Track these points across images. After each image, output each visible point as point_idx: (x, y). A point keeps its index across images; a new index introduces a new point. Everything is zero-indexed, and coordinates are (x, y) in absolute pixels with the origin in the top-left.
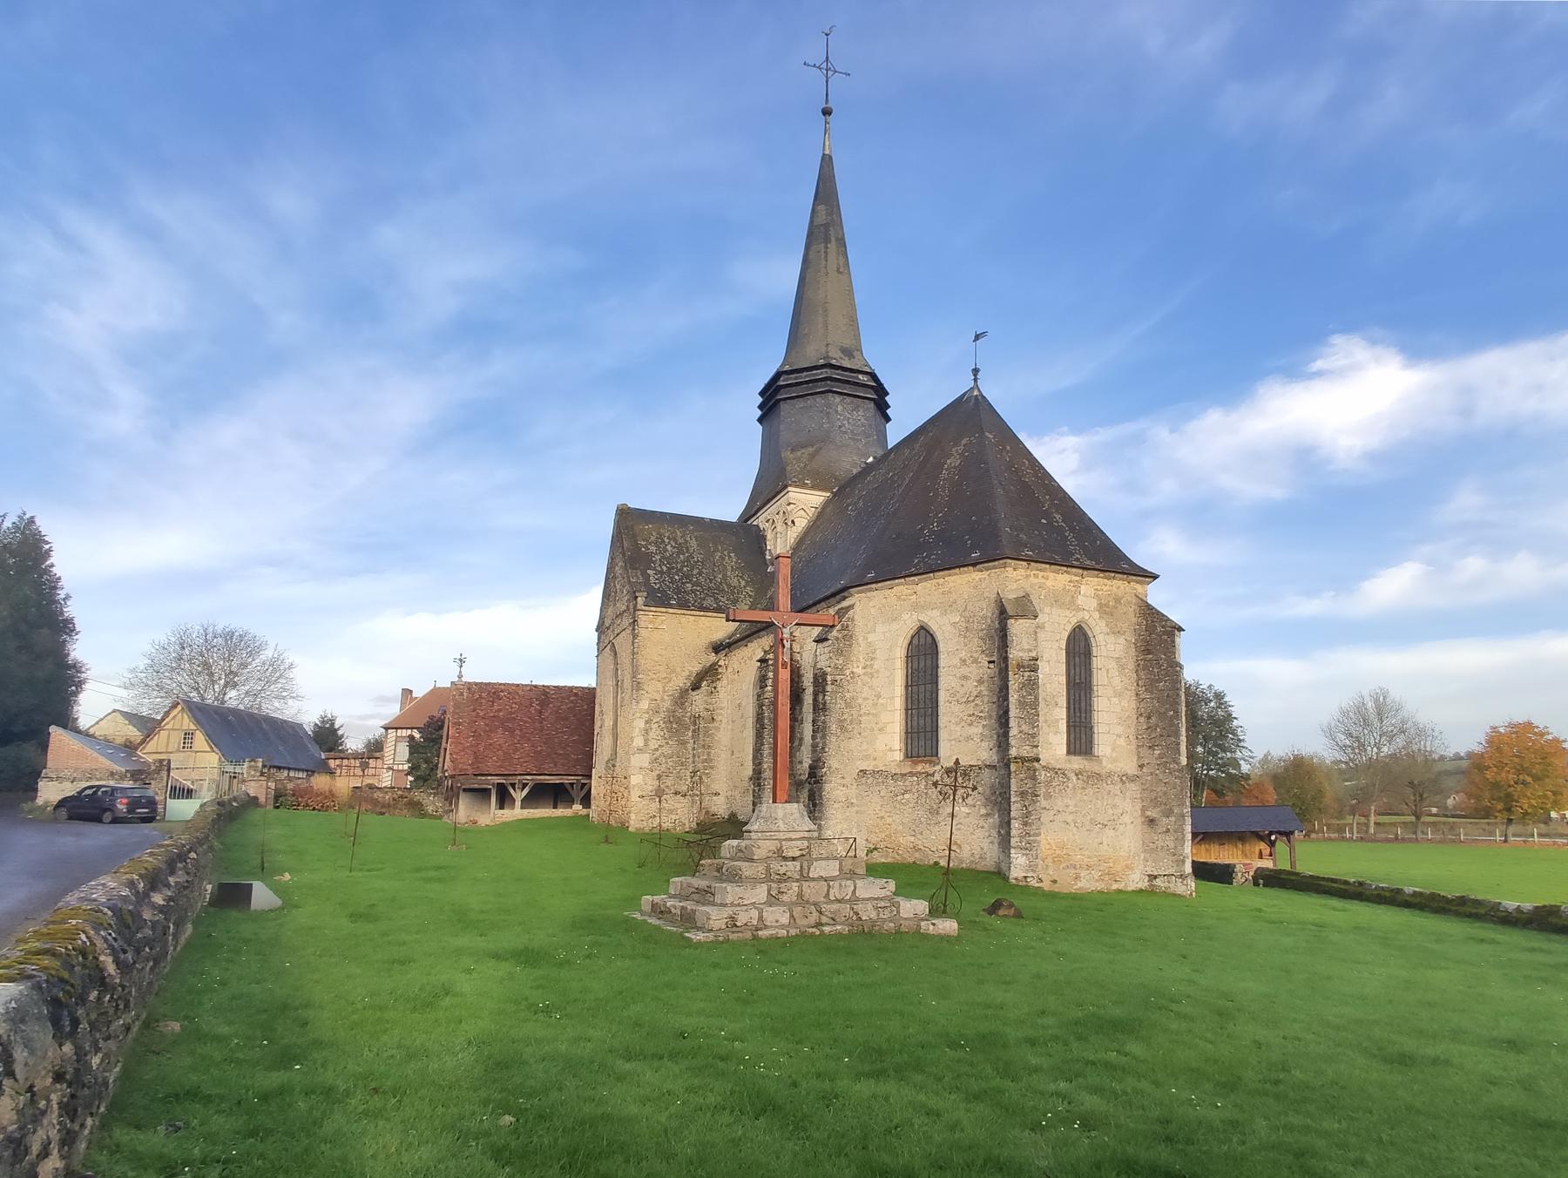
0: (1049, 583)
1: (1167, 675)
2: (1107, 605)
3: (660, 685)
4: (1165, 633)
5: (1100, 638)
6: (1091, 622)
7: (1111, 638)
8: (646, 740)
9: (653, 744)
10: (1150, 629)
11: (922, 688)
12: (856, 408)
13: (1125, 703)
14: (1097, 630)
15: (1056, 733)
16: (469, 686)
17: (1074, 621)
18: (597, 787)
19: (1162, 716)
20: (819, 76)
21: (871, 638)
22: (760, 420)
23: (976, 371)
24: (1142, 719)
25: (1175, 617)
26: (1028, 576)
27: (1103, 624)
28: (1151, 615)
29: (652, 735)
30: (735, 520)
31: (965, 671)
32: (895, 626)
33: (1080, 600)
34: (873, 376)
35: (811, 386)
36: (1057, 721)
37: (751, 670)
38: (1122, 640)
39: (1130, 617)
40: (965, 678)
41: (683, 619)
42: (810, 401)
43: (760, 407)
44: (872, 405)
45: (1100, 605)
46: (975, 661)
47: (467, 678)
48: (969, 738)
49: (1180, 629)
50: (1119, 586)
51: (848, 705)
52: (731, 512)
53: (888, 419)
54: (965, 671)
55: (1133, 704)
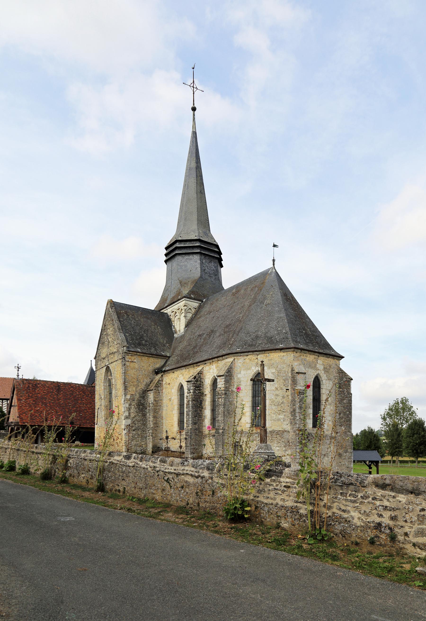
0: (308, 359)
1: (347, 397)
2: (326, 368)
3: (134, 389)
4: (346, 381)
5: (324, 381)
6: (321, 375)
7: (328, 382)
8: (129, 413)
9: (132, 415)
10: (341, 379)
11: (257, 398)
12: (210, 262)
13: (332, 408)
14: (323, 378)
15: (309, 419)
16: (23, 380)
17: (316, 374)
18: (99, 433)
19: (345, 413)
20: (190, 90)
21: (239, 376)
22: (166, 261)
23: (274, 260)
24: (337, 414)
25: (352, 376)
26: (301, 356)
27: (325, 375)
28: (342, 373)
29: (132, 411)
30: (153, 308)
31: (277, 392)
32: (249, 372)
33: (318, 366)
34: (217, 246)
35: (194, 250)
36: (310, 414)
37: (105, 370)
38: (331, 383)
39: (334, 373)
40: (277, 395)
41: (143, 358)
42: (191, 257)
43: (166, 255)
44: (217, 261)
45: (324, 368)
46: (282, 389)
47: (24, 378)
48: (279, 420)
49: (352, 379)
50: (331, 361)
51: (231, 404)
52: (151, 303)
53: (222, 266)
54: (277, 392)
55: (334, 408)
